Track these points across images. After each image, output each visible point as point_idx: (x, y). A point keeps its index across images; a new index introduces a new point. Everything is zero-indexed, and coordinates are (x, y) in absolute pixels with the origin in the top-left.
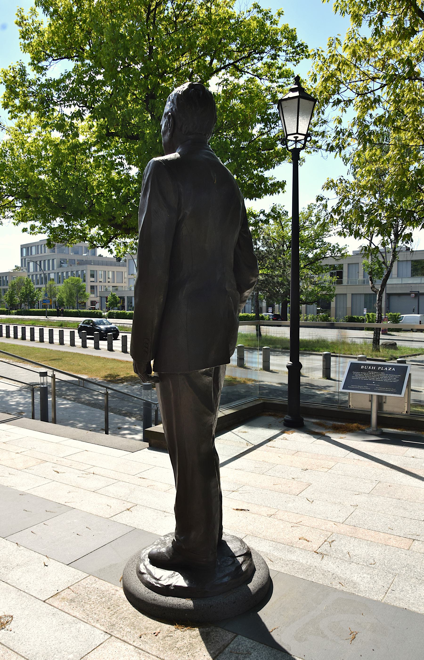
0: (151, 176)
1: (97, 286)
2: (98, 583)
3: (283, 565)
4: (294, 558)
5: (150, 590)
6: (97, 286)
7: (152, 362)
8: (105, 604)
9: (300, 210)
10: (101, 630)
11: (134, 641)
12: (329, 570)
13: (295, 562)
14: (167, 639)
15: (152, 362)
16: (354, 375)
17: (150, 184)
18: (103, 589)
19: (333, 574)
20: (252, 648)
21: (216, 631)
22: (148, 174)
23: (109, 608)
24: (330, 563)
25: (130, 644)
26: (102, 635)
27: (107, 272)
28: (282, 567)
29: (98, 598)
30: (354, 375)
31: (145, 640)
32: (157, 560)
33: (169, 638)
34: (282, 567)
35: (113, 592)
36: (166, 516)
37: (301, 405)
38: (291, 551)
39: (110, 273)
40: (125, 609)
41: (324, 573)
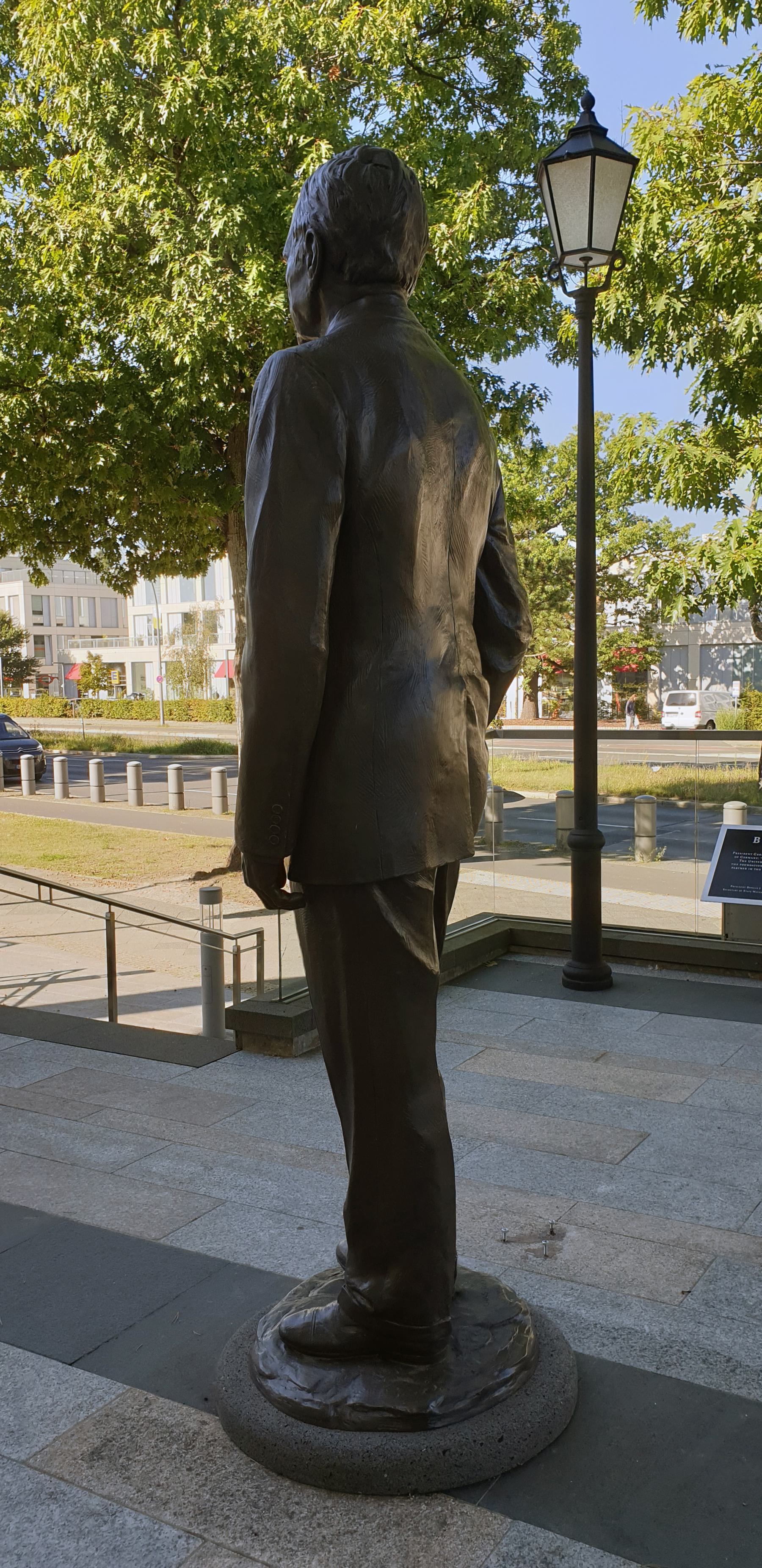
0: (276, 396)
1: (50, 636)
2: (154, 1406)
3: (606, 1342)
4: (629, 1322)
5: (290, 1419)
6: (50, 636)
7: (287, 861)
8: (177, 1460)
9: (602, 455)
10: (178, 1528)
11: (263, 1551)
12: (718, 1349)
13: (631, 1332)
14: (344, 1539)
15: (287, 861)
16: (737, 861)
17: (274, 416)
18: (170, 1420)
19: (728, 1361)
20: (553, 1553)
21: (461, 1513)
22: (268, 391)
23: (189, 1469)
24: (718, 1331)
25: (253, 1559)
26: (182, 1541)
27: (75, 600)
28: (604, 1345)
29: (161, 1445)
30: (737, 861)
31: (290, 1545)
32: (297, 1345)
33: (347, 1538)
34: (604, 1345)
35: (194, 1426)
36: (301, 1228)
37: (604, 935)
38: (619, 1305)
39: (84, 602)
40: (231, 1469)
41: (708, 1357)
